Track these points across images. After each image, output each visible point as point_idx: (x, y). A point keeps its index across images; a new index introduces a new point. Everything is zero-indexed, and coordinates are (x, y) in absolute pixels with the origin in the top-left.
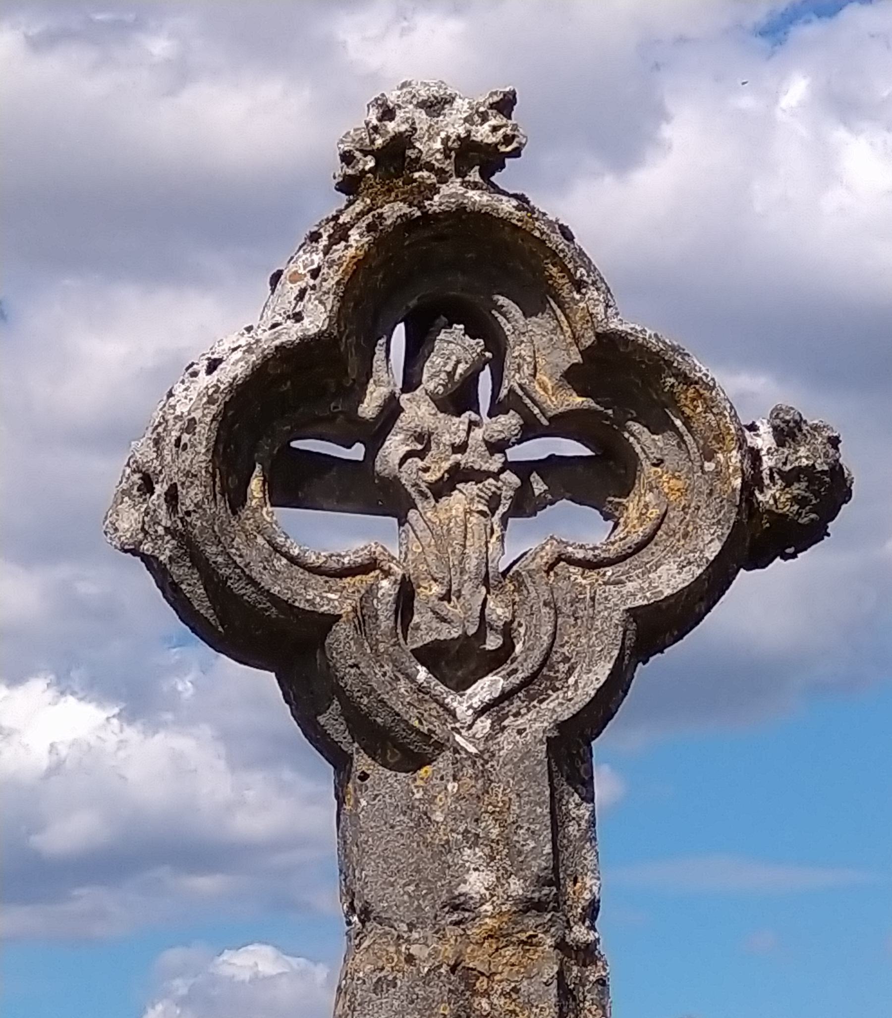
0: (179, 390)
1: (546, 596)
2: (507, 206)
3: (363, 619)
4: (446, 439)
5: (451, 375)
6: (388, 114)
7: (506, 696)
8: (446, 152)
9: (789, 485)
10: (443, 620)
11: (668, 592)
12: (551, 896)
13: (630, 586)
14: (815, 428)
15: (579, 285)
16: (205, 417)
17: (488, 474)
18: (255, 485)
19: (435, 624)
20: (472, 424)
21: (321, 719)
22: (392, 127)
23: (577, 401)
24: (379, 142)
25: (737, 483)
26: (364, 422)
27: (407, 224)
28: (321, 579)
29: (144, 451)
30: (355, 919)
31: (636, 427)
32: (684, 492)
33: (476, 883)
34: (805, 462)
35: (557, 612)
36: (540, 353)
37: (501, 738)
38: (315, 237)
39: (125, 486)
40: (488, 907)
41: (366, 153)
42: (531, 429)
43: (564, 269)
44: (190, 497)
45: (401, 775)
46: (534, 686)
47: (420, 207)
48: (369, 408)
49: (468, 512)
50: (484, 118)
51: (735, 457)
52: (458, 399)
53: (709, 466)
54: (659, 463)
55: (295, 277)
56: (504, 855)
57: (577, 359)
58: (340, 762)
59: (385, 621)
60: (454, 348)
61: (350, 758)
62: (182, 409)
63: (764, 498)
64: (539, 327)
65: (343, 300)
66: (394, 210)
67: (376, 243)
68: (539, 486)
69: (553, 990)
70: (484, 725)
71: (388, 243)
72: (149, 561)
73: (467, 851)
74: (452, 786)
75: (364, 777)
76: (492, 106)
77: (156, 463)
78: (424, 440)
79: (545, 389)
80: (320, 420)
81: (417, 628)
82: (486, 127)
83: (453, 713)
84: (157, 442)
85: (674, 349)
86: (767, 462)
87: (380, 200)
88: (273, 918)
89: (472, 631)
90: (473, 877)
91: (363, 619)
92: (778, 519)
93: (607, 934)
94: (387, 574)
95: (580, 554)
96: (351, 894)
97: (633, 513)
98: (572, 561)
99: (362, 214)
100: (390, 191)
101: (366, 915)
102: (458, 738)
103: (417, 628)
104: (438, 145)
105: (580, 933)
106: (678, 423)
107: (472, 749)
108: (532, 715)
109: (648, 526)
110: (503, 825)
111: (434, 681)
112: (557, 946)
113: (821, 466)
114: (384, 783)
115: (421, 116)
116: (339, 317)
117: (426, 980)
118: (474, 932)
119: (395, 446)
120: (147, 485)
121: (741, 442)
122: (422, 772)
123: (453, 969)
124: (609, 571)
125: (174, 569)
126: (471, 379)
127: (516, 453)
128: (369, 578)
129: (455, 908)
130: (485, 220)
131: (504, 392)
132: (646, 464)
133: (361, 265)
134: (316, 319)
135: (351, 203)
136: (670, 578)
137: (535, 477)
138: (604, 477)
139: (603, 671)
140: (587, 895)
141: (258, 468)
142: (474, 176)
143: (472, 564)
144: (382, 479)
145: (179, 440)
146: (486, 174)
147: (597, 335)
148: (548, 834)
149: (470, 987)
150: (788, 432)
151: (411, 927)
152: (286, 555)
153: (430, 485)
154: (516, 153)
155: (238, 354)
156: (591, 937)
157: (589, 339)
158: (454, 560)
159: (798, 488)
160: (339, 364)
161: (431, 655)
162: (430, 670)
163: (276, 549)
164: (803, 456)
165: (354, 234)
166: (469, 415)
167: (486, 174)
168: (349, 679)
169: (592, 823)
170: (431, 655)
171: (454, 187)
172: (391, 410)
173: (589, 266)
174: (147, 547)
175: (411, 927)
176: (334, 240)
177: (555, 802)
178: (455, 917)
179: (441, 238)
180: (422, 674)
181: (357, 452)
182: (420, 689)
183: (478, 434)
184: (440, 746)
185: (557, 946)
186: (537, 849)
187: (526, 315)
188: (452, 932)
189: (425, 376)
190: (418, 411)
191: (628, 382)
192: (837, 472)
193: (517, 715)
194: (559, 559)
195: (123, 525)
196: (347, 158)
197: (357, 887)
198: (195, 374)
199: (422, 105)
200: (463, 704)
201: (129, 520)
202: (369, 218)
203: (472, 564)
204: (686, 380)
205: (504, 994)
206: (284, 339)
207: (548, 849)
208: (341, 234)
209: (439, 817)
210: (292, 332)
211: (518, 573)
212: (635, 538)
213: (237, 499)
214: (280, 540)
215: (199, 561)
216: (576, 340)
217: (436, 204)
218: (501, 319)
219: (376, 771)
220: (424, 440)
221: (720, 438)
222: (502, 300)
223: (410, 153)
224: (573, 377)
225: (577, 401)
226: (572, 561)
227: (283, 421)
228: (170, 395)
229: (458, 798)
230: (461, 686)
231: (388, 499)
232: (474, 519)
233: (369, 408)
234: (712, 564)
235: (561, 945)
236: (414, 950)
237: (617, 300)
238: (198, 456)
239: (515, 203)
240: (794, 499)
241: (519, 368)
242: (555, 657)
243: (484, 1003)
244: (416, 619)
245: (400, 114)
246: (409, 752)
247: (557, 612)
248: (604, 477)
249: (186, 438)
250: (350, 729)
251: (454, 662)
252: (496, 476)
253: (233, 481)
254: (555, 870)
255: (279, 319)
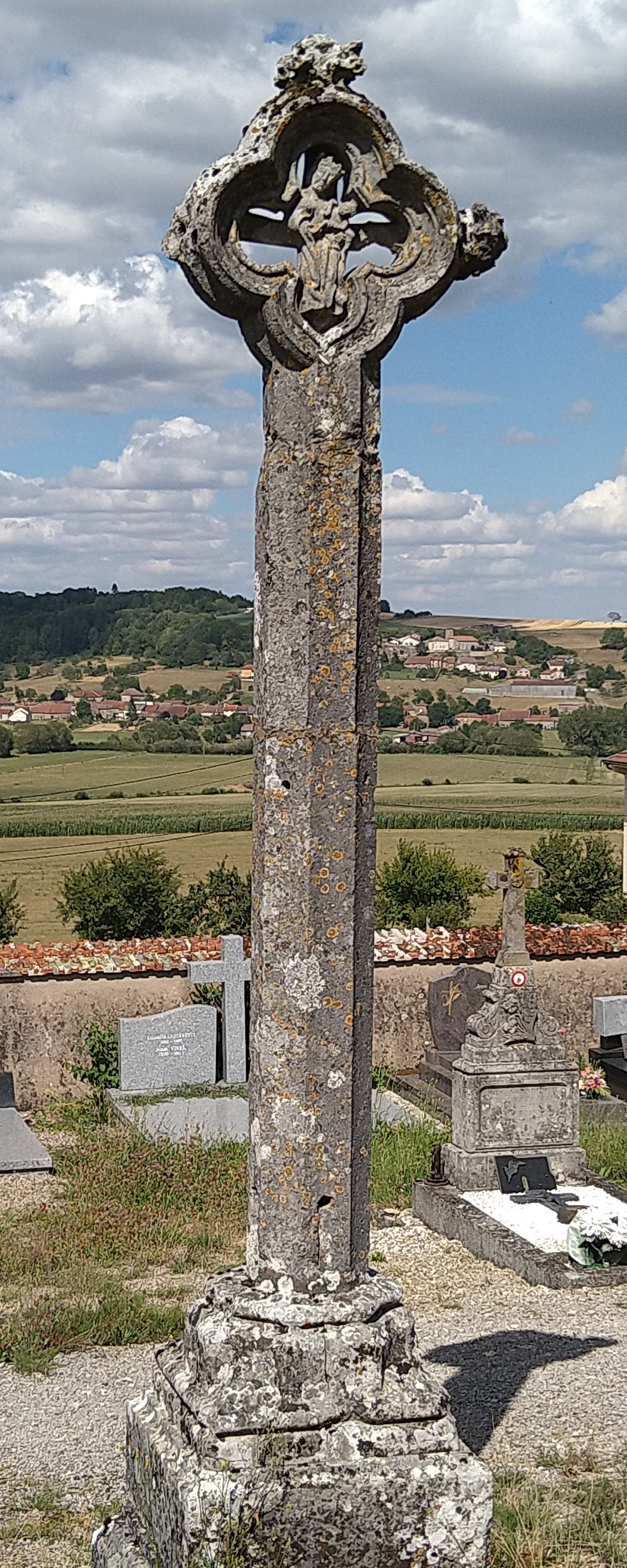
0: (199, 183)
1: (364, 290)
2: (356, 100)
3: (280, 297)
4: (322, 212)
5: (325, 181)
6: (302, 51)
7: (343, 337)
8: (328, 71)
9: (479, 241)
10: (316, 299)
11: (420, 291)
12: (359, 433)
13: (403, 288)
14: (493, 214)
15: (388, 141)
16: (212, 197)
17: (339, 230)
18: (233, 231)
19: (312, 301)
20: (334, 206)
21: (259, 344)
22: (304, 58)
23: (383, 197)
24: (297, 65)
25: (455, 240)
26: (284, 202)
27: (309, 106)
28: (261, 278)
29: (181, 211)
30: (269, 438)
31: (410, 210)
32: (430, 243)
33: (326, 425)
34: (486, 231)
35: (368, 298)
36: (367, 172)
37: (340, 357)
38: (264, 110)
39: (172, 228)
40: (330, 436)
41: (290, 70)
42: (361, 209)
43: (381, 132)
44: (203, 236)
45: (294, 373)
46: (356, 334)
47: (316, 99)
48: (287, 196)
49: (330, 248)
50: (347, 55)
51: (455, 227)
52: (327, 193)
53: (443, 231)
54: (420, 228)
55: (255, 130)
56: (339, 412)
57: (384, 176)
58: (267, 365)
59: (290, 299)
60: (327, 168)
61: (271, 363)
62: (201, 192)
63: (467, 247)
64: (368, 158)
65: (277, 143)
66: (303, 100)
67: (293, 116)
68: (363, 236)
69: (358, 475)
70: (332, 350)
71: (298, 114)
72: (183, 265)
73: (322, 410)
74: (317, 379)
75: (277, 372)
76: (352, 50)
77: (187, 218)
78: (311, 212)
79: (368, 189)
80: (263, 201)
81: (304, 303)
82: (348, 60)
83: (318, 344)
84: (188, 207)
85: (430, 174)
86: (469, 230)
87: (296, 94)
88: (199, 406)
89: (329, 305)
90: (324, 422)
91: (280, 297)
92: (473, 257)
93: (382, 450)
94: (292, 276)
95: (380, 271)
96: (268, 426)
97: (406, 251)
98: (376, 274)
99: (288, 101)
100: (301, 90)
101: (275, 437)
102: (321, 357)
103: (304, 303)
104: (324, 67)
105: (370, 449)
106: (429, 209)
107: (327, 362)
108: (355, 347)
109: (412, 259)
110: (339, 398)
111: (311, 329)
112: (360, 455)
113: (494, 233)
114: (286, 376)
115: (317, 52)
116: (274, 152)
117: (301, 468)
118: (324, 447)
119: (298, 215)
120: (183, 229)
121: (458, 220)
122: (303, 372)
123: (313, 464)
124: (393, 279)
125: (193, 269)
126: (334, 183)
127: (352, 221)
128: (283, 278)
129: (316, 436)
130: (345, 106)
131: (349, 190)
132: (413, 229)
133: (286, 126)
134: (264, 153)
135: (282, 94)
136: (422, 284)
137: (361, 232)
138: (393, 234)
139: (388, 327)
140: (374, 432)
141: (235, 223)
142: (341, 84)
143: (330, 273)
144: (292, 230)
145: (198, 209)
146: (347, 83)
147: (395, 166)
148: (359, 403)
149: (320, 472)
150: (480, 216)
151: (295, 443)
152: (246, 265)
153: (314, 235)
154: (361, 74)
155: (228, 168)
156: (376, 451)
157: (390, 167)
158: (322, 271)
159: (482, 243)
160: (275, 174)
161: (309, 316)
162: (310, 323)
163: (241, 262)
164: (486, 228)
165: (284, 111)
166: (333, 201)
167: (347, 83)
168: (273, 326)
169: (379, 398)
170: (309, 316)
171: (331, 89)
172: (297, 196)
173: (393, 133)
174: (182, 258)
175: (295, 443)
176: (274, 113)
177: (363, 389)
178: (316, 440)
179: (323, 114)
180: (306, 325)
181: (280, 216)
182: (304, 332)
183: (336, 210)
184: (312, 360)
185: (360, 455)
186: (353, 408)
187: (362, 153)
188: (314, 447)
189: (314, 180)
190: (309, 198)
191: (409, 189)
192: (501, 234)
193: (348, 346)
194: (371, 272)
195: (171, 247)
196: (281, 71)
197: (271, 423)
198: (207, 176)
199: (318, 47)
200: (323, 340)
201: (174, 244)
202: (291, 104)
203: (330, 273)
204: (434, 189)
205: (335, 476)
206: (249, 161)
207: (359, 410)
208: (277, 110)
209: (310, 393)
210: (254, 158)
211: (351, 279)
212: (407, 264)
213: (225, 238)
214: (243, 258)
215: (206, 267)
216: (385, 167)
217: (322, 98)
218: (350, 155)
219: (283, 370)
220: (311, 212)
221: (449, 218)
222: (351, 146)
223: (312, 72)
224: (381, 185)
225: (383, 197)
226: (376, 274)
227: (247, 200)
228: (195, 185)
229: (319, 385)
230: (322, 331)
231: (295, 240)
232: (333, 252)
233: (287, 196)
234: (441, 279)
235: (362, 455)
236: (297, 454)
237: (405, 150)
238: (207, 217)
239: (360, 99)
240: (481, 249)
241: (357, 179)
242: (366, 320)
243: (326, 480)
244: (304, 298)
245: (307, 52)
246: (298, 361)
247: (368, 298)
248: (393, 234)
249: (202, 207)
250: (276, 353)
251: (322, 319)
252: (344, 231)
253: (223, 229)
254: (361, 420)
255: (247, 151)
